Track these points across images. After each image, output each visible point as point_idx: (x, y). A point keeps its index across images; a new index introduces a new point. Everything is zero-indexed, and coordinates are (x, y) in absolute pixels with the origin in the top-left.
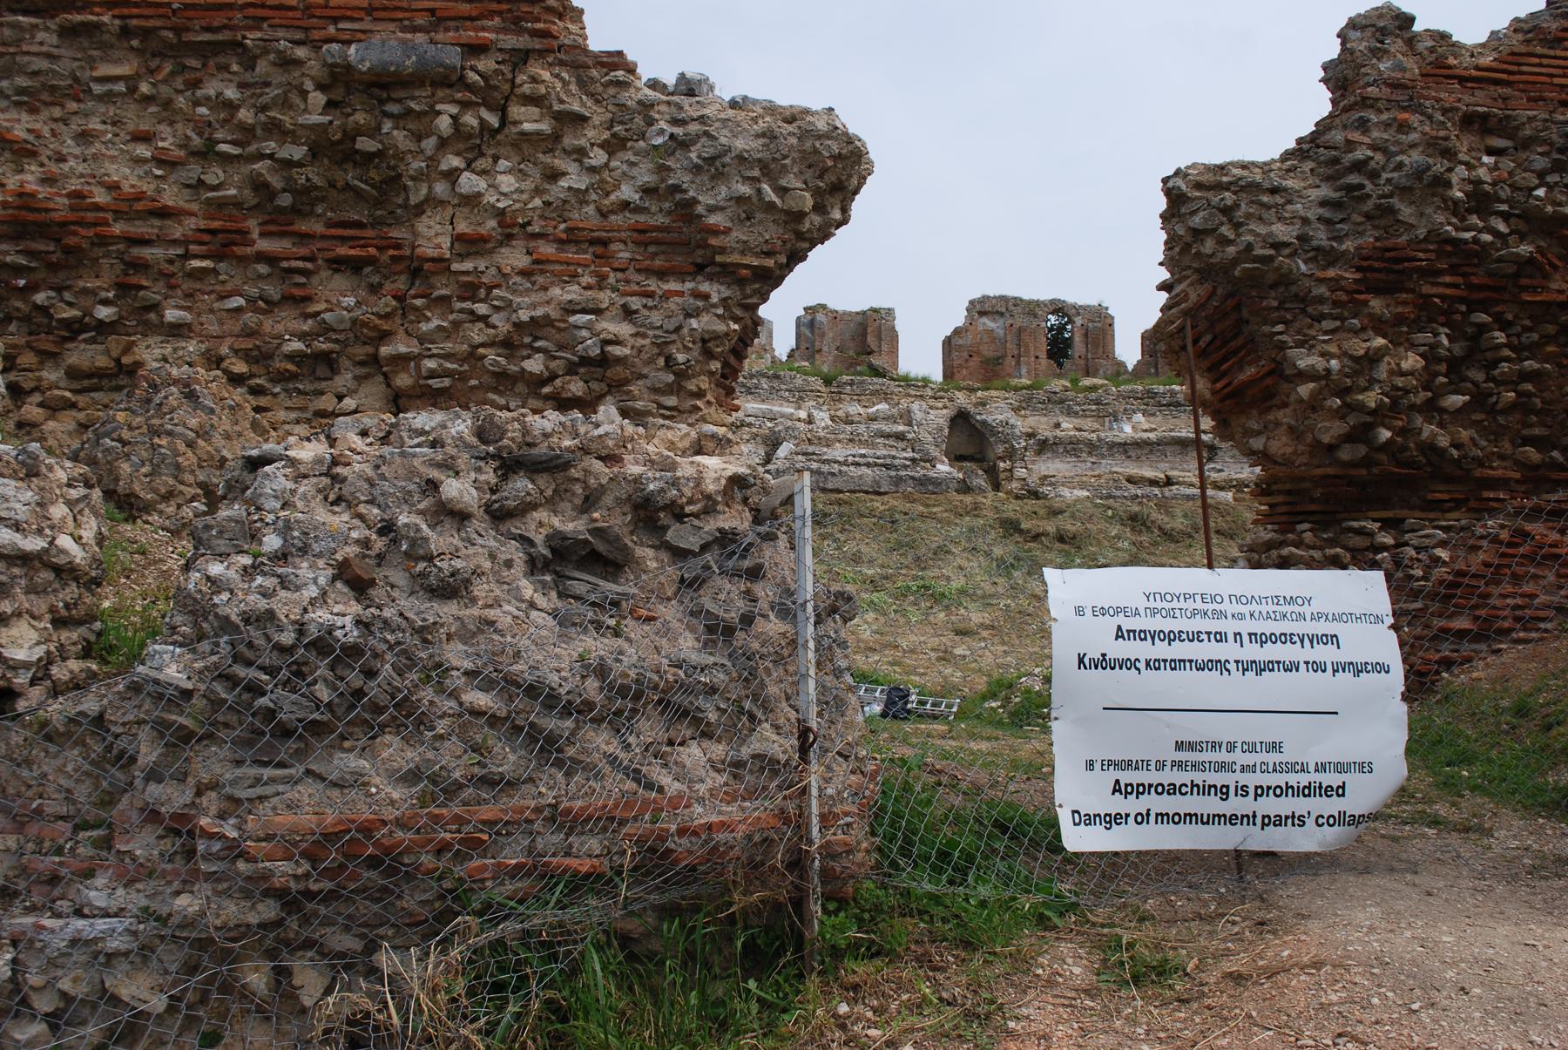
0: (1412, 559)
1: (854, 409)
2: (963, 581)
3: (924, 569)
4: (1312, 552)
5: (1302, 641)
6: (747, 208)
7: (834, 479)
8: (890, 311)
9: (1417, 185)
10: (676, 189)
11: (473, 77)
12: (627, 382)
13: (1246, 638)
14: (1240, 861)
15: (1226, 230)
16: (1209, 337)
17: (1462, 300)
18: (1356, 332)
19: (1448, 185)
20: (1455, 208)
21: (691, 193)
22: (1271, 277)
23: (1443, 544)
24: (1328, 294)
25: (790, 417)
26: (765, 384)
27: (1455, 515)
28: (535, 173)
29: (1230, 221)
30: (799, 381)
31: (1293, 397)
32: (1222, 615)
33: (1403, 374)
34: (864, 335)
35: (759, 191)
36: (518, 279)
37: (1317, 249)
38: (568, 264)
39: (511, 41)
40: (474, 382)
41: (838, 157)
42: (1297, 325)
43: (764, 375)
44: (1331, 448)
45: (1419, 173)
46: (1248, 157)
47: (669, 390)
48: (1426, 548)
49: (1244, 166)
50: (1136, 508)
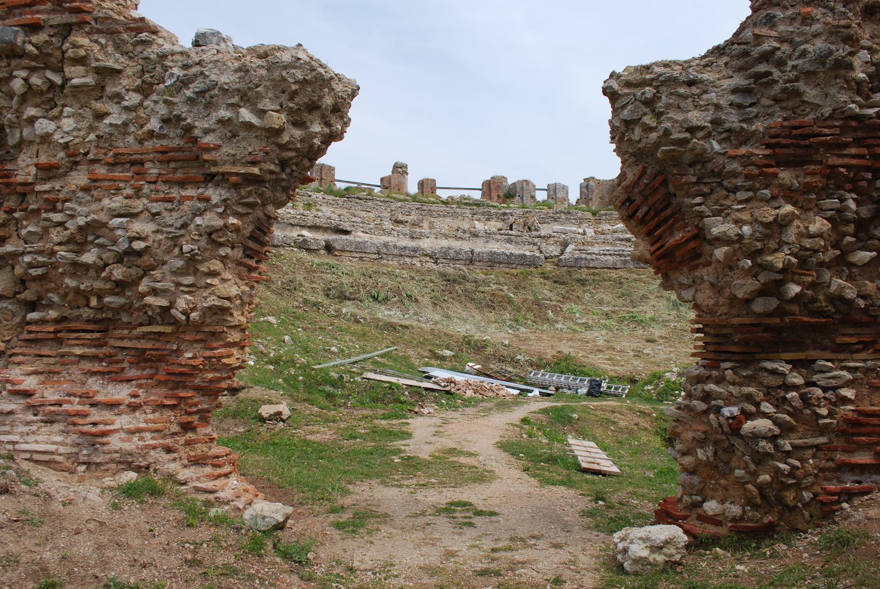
0: (818, 399)
3: (634, 307)
4: (731, 388)
9: (821, 69)
10: (179, 118)
11: (30, 48)
16: (644, 209)
17: (867, 169)
19: (850, 67)
20: (858, 87)
21: (189, 121)
22: (688, 157)
23: (848, 384)
24: (740, 169)
27: (863, 355)
28: (88, 113)
29: (653, 111)
30: (580, 214)
31: (713, 257)
33: (812, 236)
36: (80, 194)
37: (729, 130)
38: (115, 181)
39: (57, 19)
40: (60, 270)
41: (304, 82)
42: (714, 196)
43: (562, 212)
44: (748, 301)
45: (822, 59)
48: (834, 389)
49: (666, 65)
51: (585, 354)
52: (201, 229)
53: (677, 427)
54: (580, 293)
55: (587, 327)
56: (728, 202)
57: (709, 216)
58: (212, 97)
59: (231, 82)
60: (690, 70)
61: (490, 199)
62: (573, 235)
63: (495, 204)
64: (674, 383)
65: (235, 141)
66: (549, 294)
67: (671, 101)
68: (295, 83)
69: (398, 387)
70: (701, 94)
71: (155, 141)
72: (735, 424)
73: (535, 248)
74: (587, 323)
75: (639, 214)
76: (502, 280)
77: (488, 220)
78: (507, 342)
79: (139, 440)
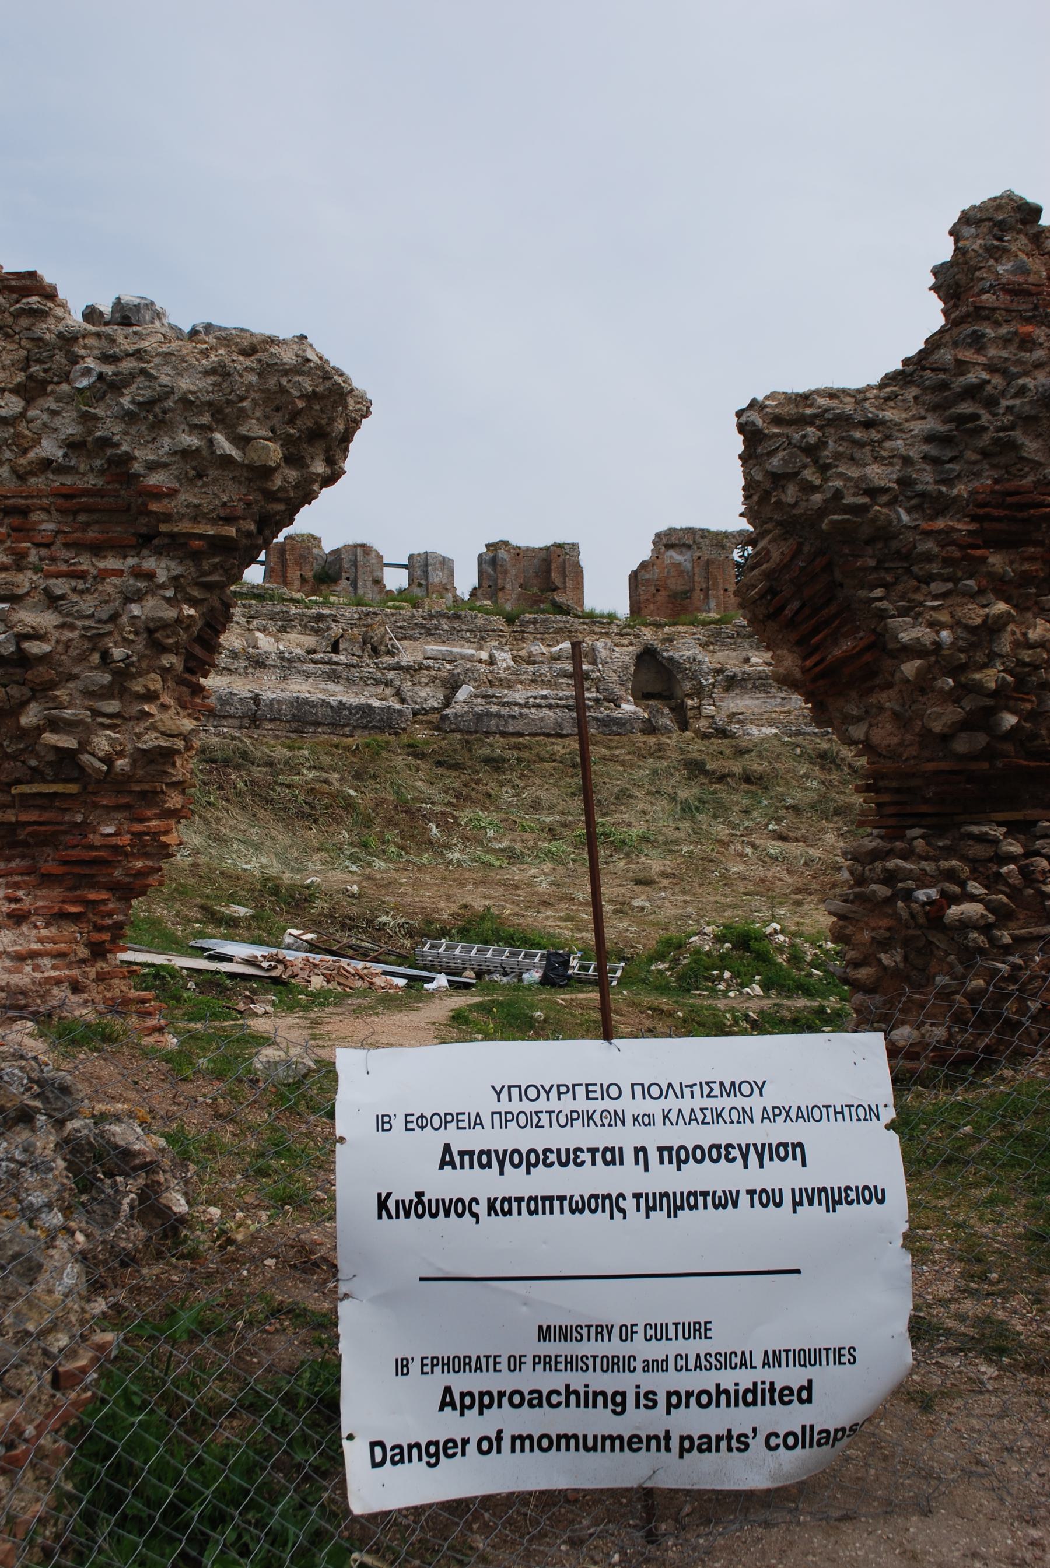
1: (538, 648)
2: (644, 828)
4: (924, 864)
5: (745, 1157)
6: (197, 464)
7: (514, 722)
8: (574, 546)
10: (106, 442)
12: (53, 685)
13: (653, 1156)
14: (649, 1505)
15: (809, 474)
16: (796, 605)
18: (972, 596)
21: (125, 448)
24: (936, 549)
25: (470, 659)
26: (445, 625)
29: (816, 462)
30: (480, 621)
31: (898, 675)
32: (617, 1118)
34: (548, 571)
35: (211, 442)
37: (923, 495)
41: (312, 397)
42: (900, 588)
44: (945, 738)
46: (838, 384)
47: (106, 693)
49: (833, 394)
50: (825, 746)
51: (517, 909)
52: (138, 623)
53: (845, 927)
54: (492, 787)
55: (513, 856)
56: (919, 597)
57: (893, 616)
58: (165, 412)
59: (200, 390)
60: (867, 404)
61: (285, 583)
62: (469, 665)
63: (298, 596)
64: (708, 954)
65: (200, 483)
66: (427, 790)
67: (841, 449)
68: (301, 397)
69: (173, 972)
70: (883, 441)
71: (51, 476)
72: (935, 911)
73: (389, 691)
74: (511, 849)
75: (788, 612)
76: (326, 760)
77: (283, 629)
78: (355, 889)
79: (33, 970)
